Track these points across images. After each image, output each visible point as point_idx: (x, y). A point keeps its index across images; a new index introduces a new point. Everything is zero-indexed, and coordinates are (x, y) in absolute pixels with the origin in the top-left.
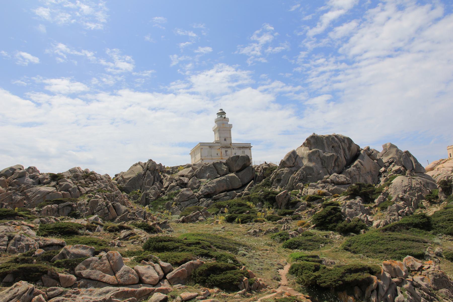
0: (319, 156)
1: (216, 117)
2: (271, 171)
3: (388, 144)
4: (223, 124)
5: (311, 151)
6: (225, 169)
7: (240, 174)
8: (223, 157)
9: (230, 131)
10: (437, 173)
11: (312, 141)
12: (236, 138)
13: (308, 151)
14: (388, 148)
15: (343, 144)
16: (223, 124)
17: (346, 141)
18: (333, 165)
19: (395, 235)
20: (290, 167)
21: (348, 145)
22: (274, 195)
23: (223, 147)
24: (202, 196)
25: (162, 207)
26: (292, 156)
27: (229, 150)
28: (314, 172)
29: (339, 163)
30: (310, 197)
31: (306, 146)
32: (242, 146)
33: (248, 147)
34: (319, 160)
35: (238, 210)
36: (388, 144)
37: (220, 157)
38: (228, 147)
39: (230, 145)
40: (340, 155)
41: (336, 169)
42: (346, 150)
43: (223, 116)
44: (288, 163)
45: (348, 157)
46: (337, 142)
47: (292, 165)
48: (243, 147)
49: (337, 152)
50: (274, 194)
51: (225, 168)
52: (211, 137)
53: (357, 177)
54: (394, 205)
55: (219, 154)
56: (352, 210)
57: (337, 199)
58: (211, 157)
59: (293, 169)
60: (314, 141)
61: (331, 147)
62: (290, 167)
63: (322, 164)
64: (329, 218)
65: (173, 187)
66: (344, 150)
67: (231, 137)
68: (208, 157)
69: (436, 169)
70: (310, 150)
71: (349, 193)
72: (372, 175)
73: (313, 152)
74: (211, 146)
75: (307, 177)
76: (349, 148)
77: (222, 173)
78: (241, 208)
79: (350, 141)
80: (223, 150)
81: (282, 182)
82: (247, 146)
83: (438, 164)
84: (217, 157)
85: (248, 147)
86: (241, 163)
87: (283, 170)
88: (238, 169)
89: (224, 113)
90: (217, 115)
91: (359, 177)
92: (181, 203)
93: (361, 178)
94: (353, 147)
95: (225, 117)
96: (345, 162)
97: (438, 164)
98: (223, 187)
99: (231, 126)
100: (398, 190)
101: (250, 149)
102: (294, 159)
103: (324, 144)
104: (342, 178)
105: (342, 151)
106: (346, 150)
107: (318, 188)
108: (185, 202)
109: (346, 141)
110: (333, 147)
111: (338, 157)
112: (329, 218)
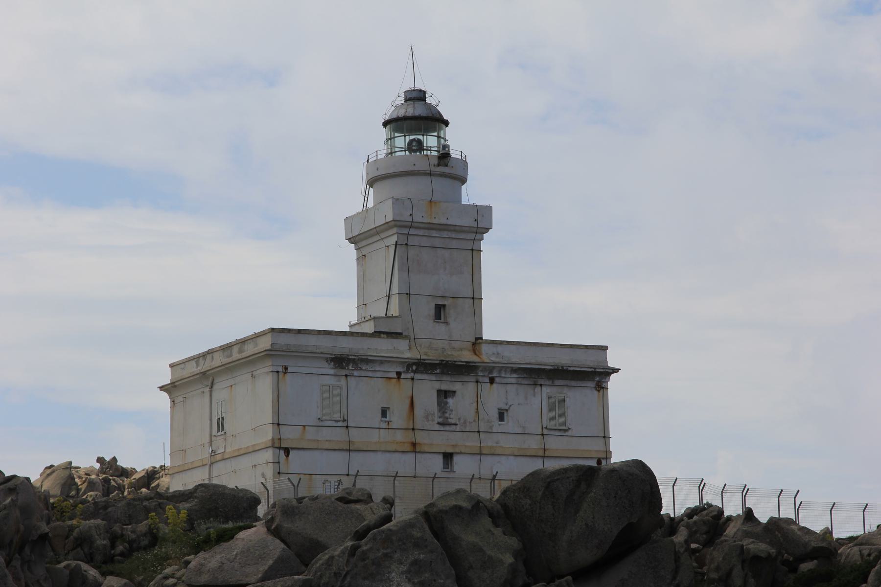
1: (376, 142)
4: (424, 203)
6: (509, 559)
8: (420, 437)
9: (476, 251)
12: (517, 307)
16: (424, 203)
27: (465, 392)
33: (583, 373)
37: (400, 436)
43: (430, 141)
52: (327, 295)
55: (398, 418)
67: (476, 299)
80: (426, 389)
82: (587, 361)
85: (583, 373)
88: (585, 556)
89: (434, 121)
90: (383, 133)
101: (601, 388)
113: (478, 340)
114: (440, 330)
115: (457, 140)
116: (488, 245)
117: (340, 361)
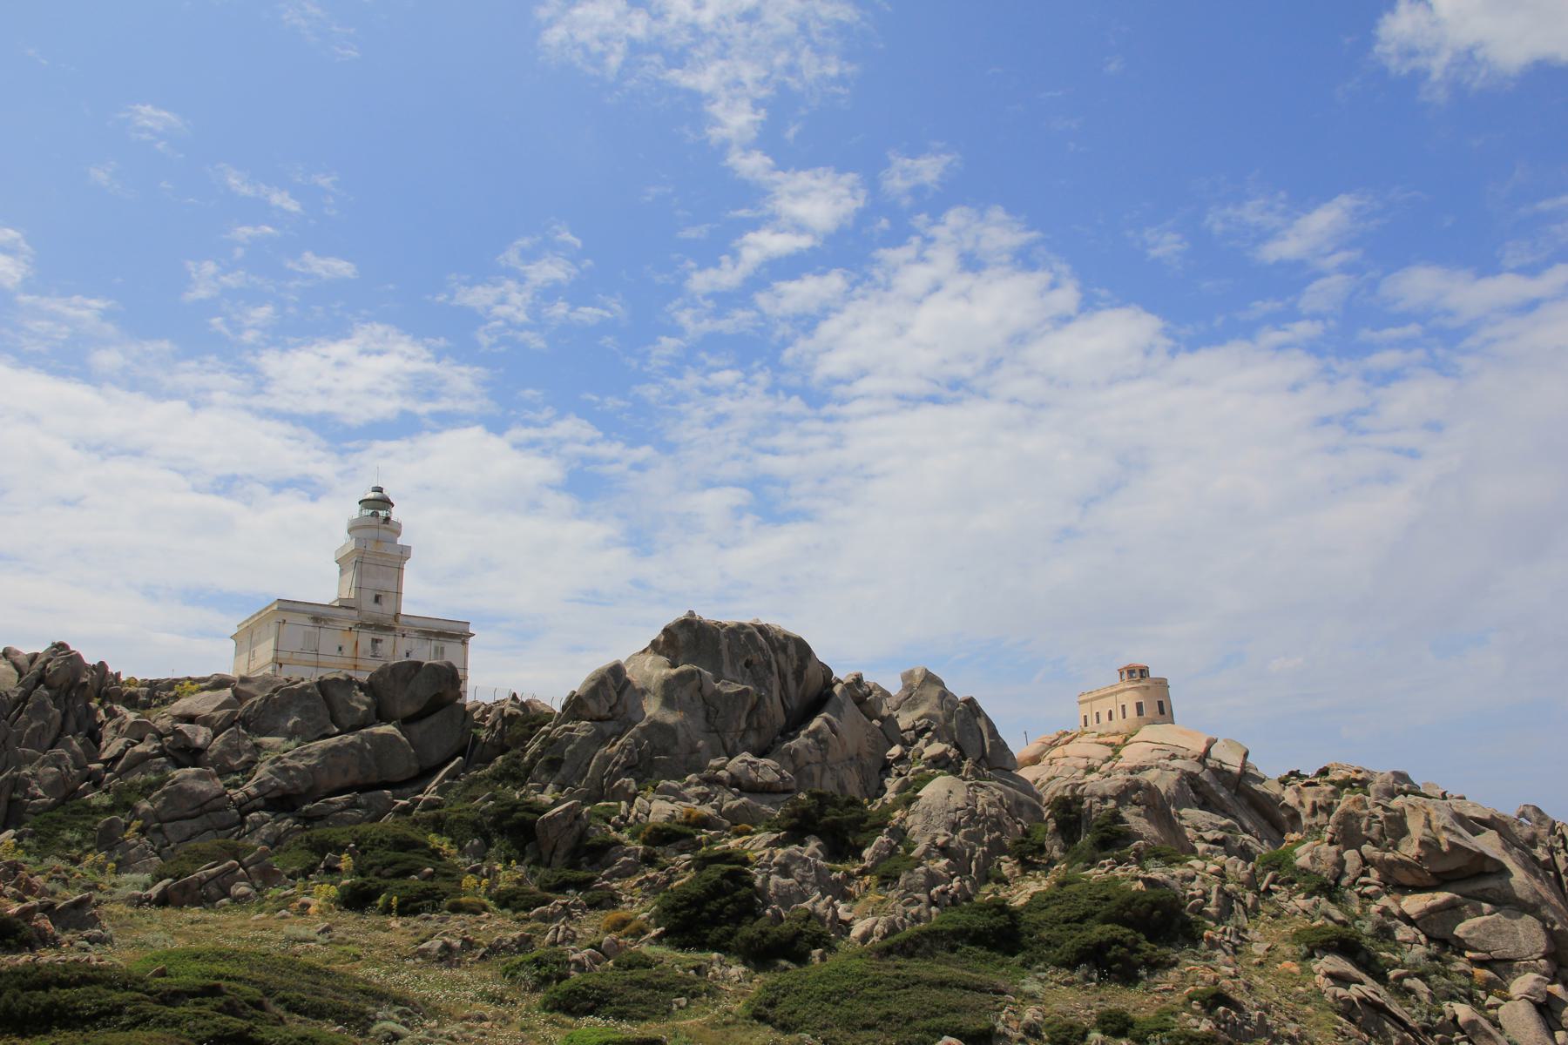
0: (700, 689)
1: (355, 511)
2: (532, 728)
3: (917, 673)
4: (377, 538)
5: (674, 672)
7: (417, 729)
8: (359, 662)
9: (401, 569)
10: (1049, 775)
11: (682, 637)
12: (420, 596)
13: (664, 671)
14: (916, 684)
15: (781, 657)
17: (792, 649)
18: (743, 725)
19: (917, 968)
20: (600, 719)
21: (796, 663)
22: (530, 816)
23: (363, 626)
24: (260, 802)
25: (78, 837)
26: (611, 681)
28: (676, 743)
29: (764, 720)
30: (655, 829)
31: (660, 653)
32: (436, 628)
33: (458, 634)
34: (699, 703)
35: (392, 864)
36: (917, 673)
38: (388, 626)
39: (391, 622)
40: (770, 692)
41: (752, 739)
42: (790, 677)
43: (382, 513)
44: (592, 704)
45: (794, 703)
46: (761, 649)
47: (604, 713)
48: (441, 635)
49: (759, 682)
50: (530, 810)
51: (361, 703)
52: (325, 585)
53: (816, 770)
54: (922, 869)
55: (348, 651)
56: (790, 881)
57: (744, 843)
58: (313, 658)
59: (608, 727)
60: (687, 640)
61: (742, 663)
62: (600, 719)
63: (707, 718)
64: (713, 906)
65: (145, 757)
66: (782, 677)
67: (399, 593)
68: (305, 657)
69: (1046, 761)
70: (673, 666)
71: (784, 824)
72: (862, 768)
73: (680, 676)
74: (319, 616)
75: (652, 761)
76: (799, 674)
77: (347, 721)
78: (404, 855)
79: (803, 649)
80: (366, 638)
81: (563, 771)
82: (456, 629)
83: (1052, 745)
84: (339, 660)
86: (423, 691)
87: (572, 730)
88: (410, 709)
89: (386, 503)
91: (823, 771)
92: (168, 826)
93: (828, 775)
94: (810, 670)
95: (387, 519)
96: (781, 719)
97: (1052, 745)
98: (346, 772)
99: (405, 553)
100: (935, 822)
101: (464, 643)
102: (614, 694)
103: (719, 652)
104: (768, 770)
105: (775, 680)
106: (790, 677)
107: (686, 800)
108: (183, 823)
109: (792, 649)
110: (748, 664)
111: (760, 698)
112: (713, 906)
113: (397, 615)
114: (377, 607)
115: (396, 514)
116: (408, 568)
117: (316, 619)
